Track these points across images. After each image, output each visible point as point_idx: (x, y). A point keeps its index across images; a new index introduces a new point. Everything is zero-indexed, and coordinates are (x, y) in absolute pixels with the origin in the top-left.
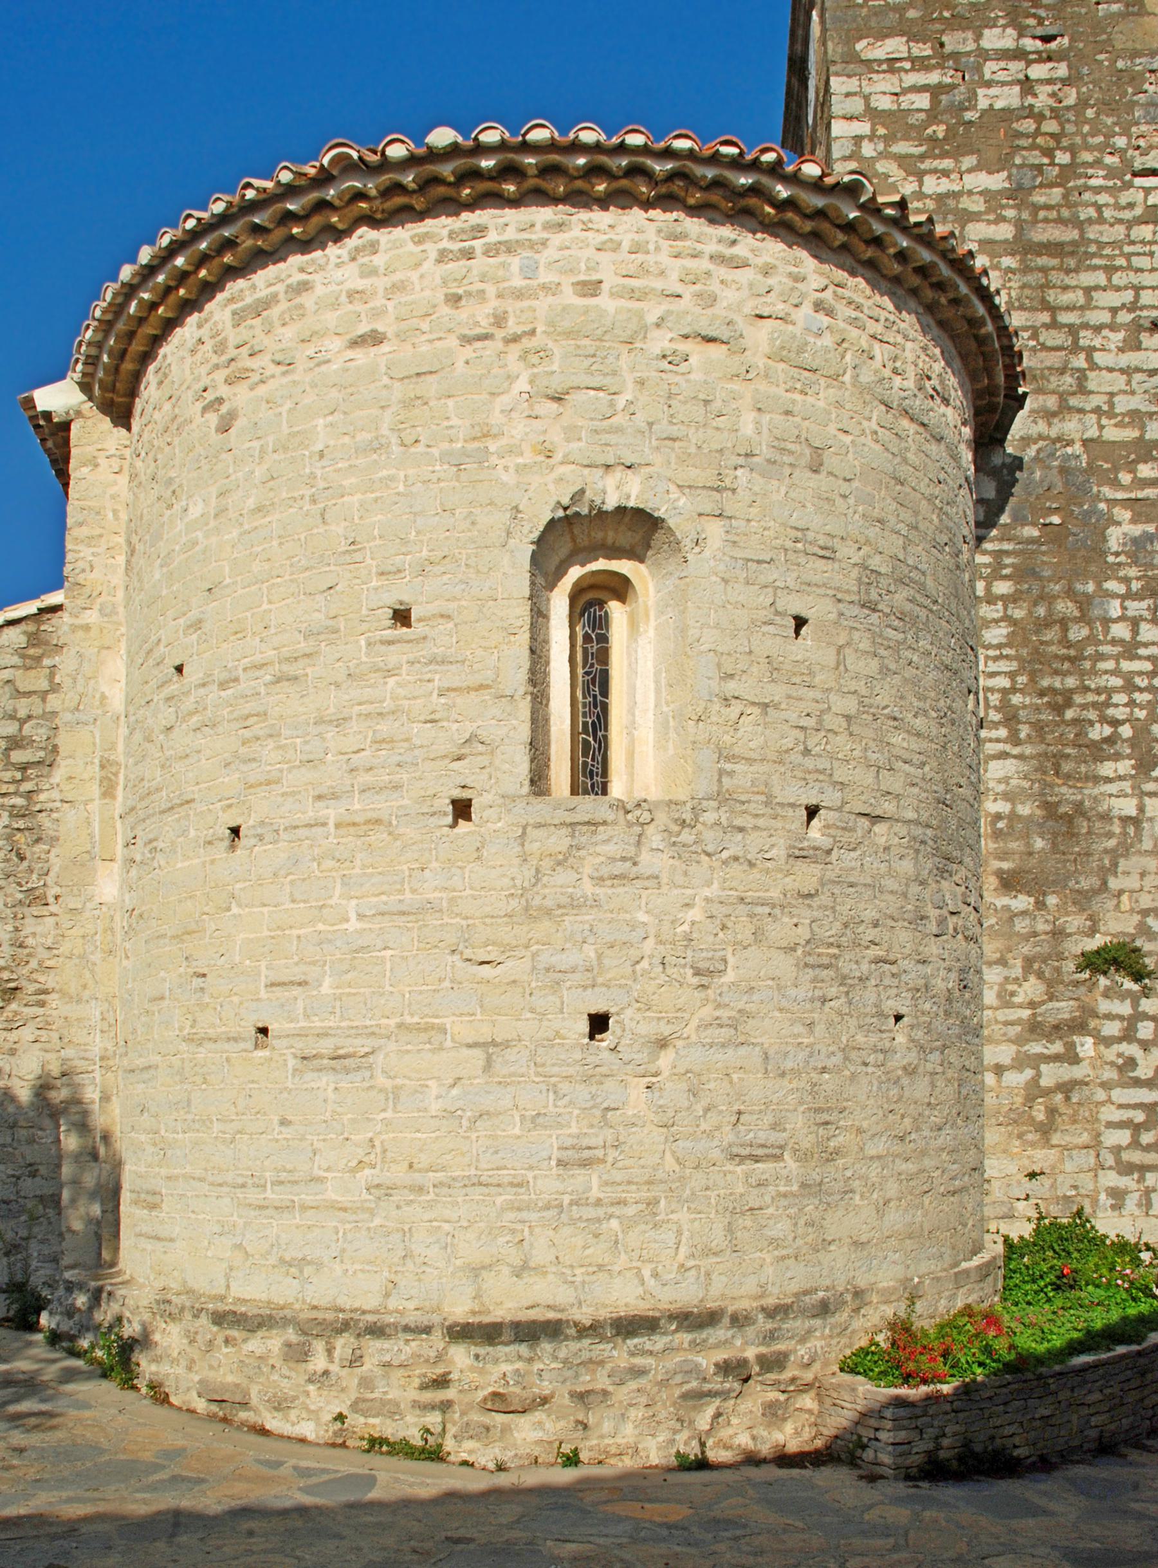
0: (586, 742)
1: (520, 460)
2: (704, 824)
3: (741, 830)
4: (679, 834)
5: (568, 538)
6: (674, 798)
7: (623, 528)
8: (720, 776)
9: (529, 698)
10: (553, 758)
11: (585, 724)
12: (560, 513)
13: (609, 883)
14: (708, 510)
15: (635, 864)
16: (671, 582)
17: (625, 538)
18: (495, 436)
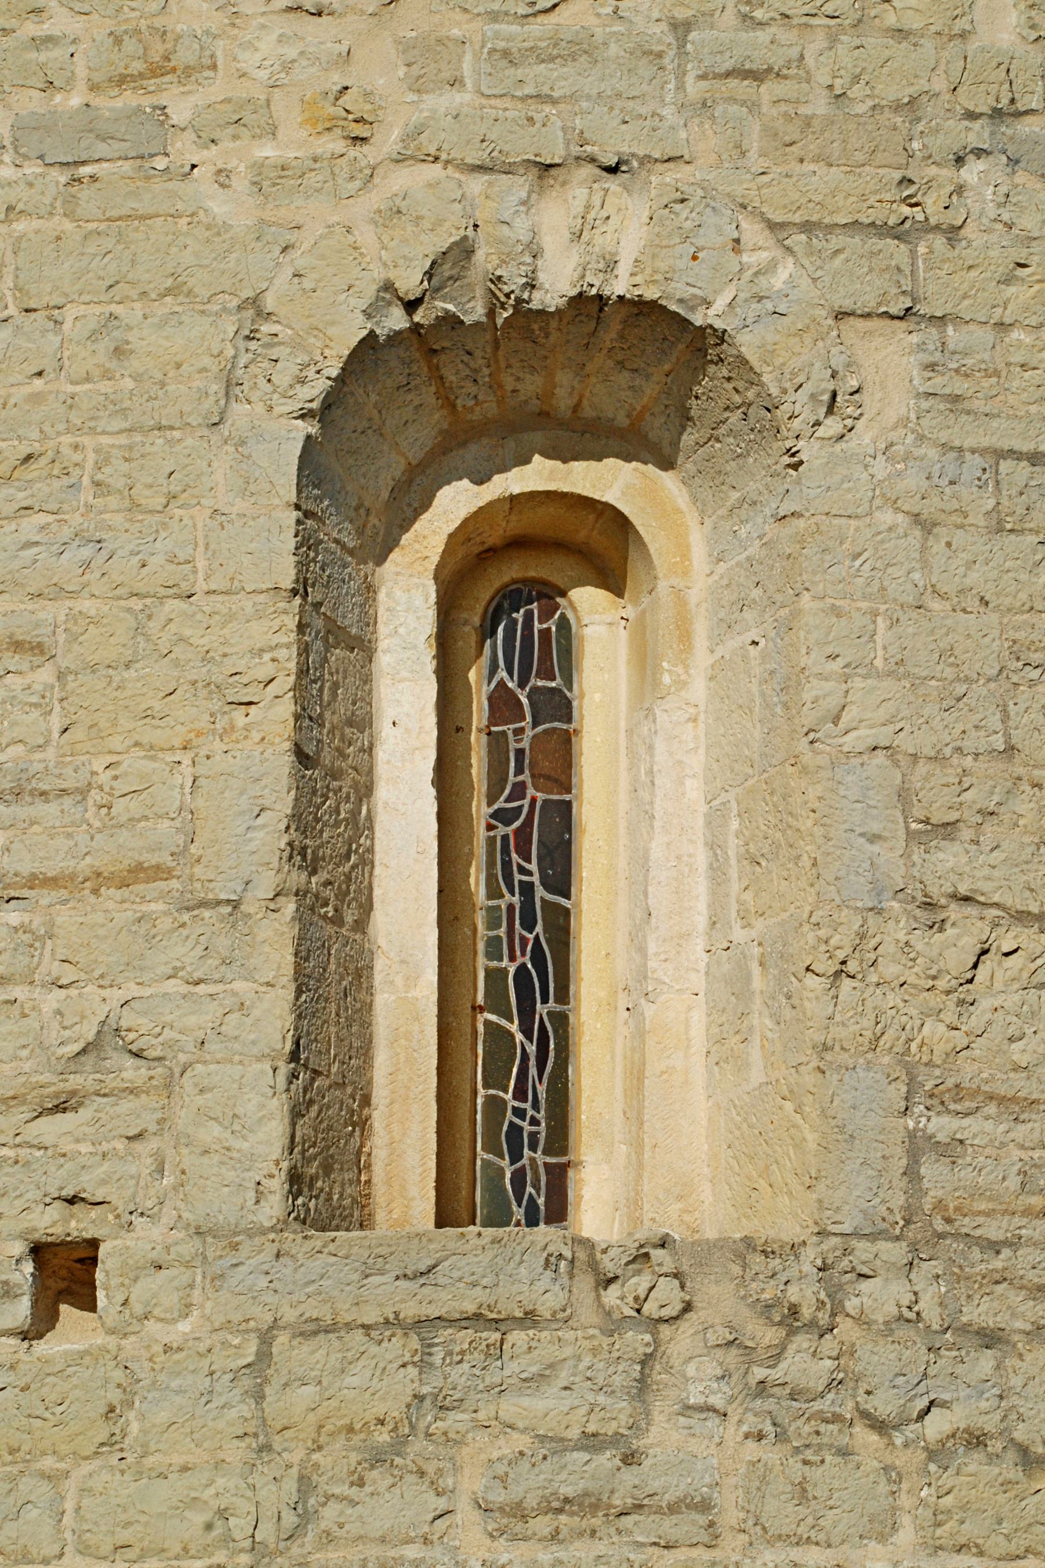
0: (497, 1035)
1: (267, 151)
2: (861, 1320)
3: (990, 1338)
4: (776, 1356)
5: (428, 395)
6: (762, 1230)
7: (599, 361)
8: (914, 1156)
9: (290, 907)
10: (380, 1094)
11: (495, 977)
12: (397, 320)
13: (542, 1525)
14: (869, 302)
15: (630, 1459)
16: (756, 526)
17: (611, 393)
18: (188, 71)
